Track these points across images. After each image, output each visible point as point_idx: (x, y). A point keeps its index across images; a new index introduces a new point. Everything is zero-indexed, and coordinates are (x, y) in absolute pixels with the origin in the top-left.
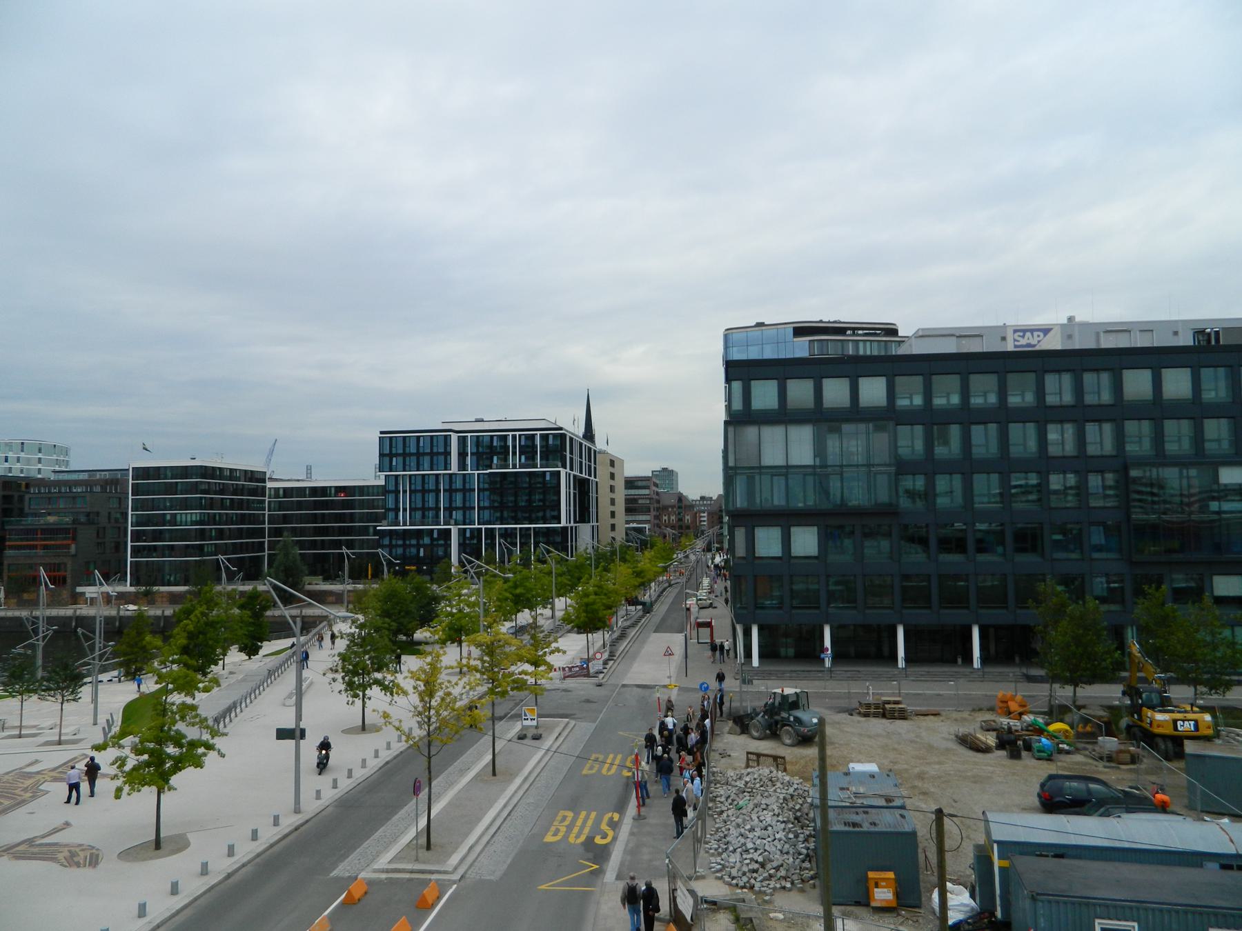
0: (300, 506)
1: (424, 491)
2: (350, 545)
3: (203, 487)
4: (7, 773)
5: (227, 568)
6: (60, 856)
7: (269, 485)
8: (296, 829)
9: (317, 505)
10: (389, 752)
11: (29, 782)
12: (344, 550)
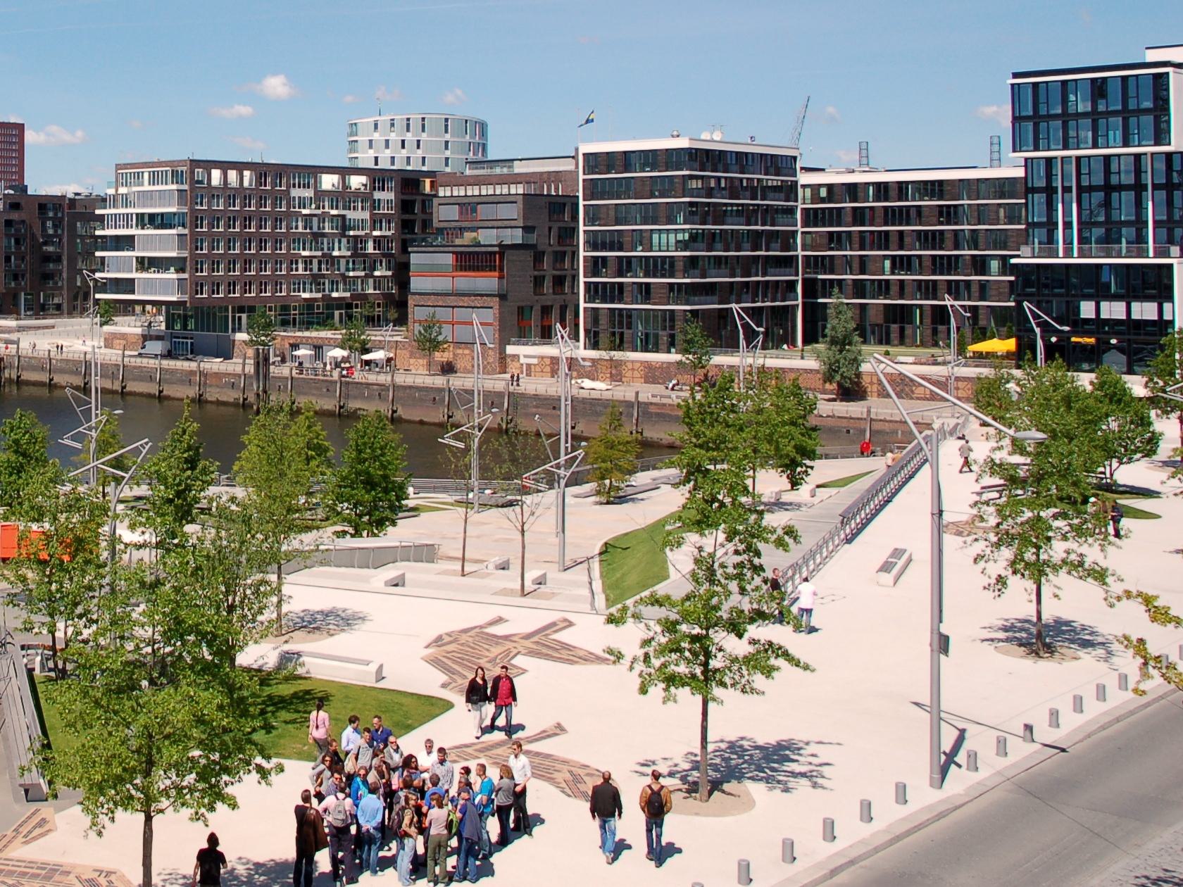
0: (859, 216)
1: (1108, 188)
2: (955, 290)
3: (694, 184)
4: (465, 631)
5: (746, 326)
6: (559, 777)
7: (804, 178)
8: (1089, 736)
9: (892, 216)
10: (1003, 762)
11: (495, 651)
12: (948, 302)
